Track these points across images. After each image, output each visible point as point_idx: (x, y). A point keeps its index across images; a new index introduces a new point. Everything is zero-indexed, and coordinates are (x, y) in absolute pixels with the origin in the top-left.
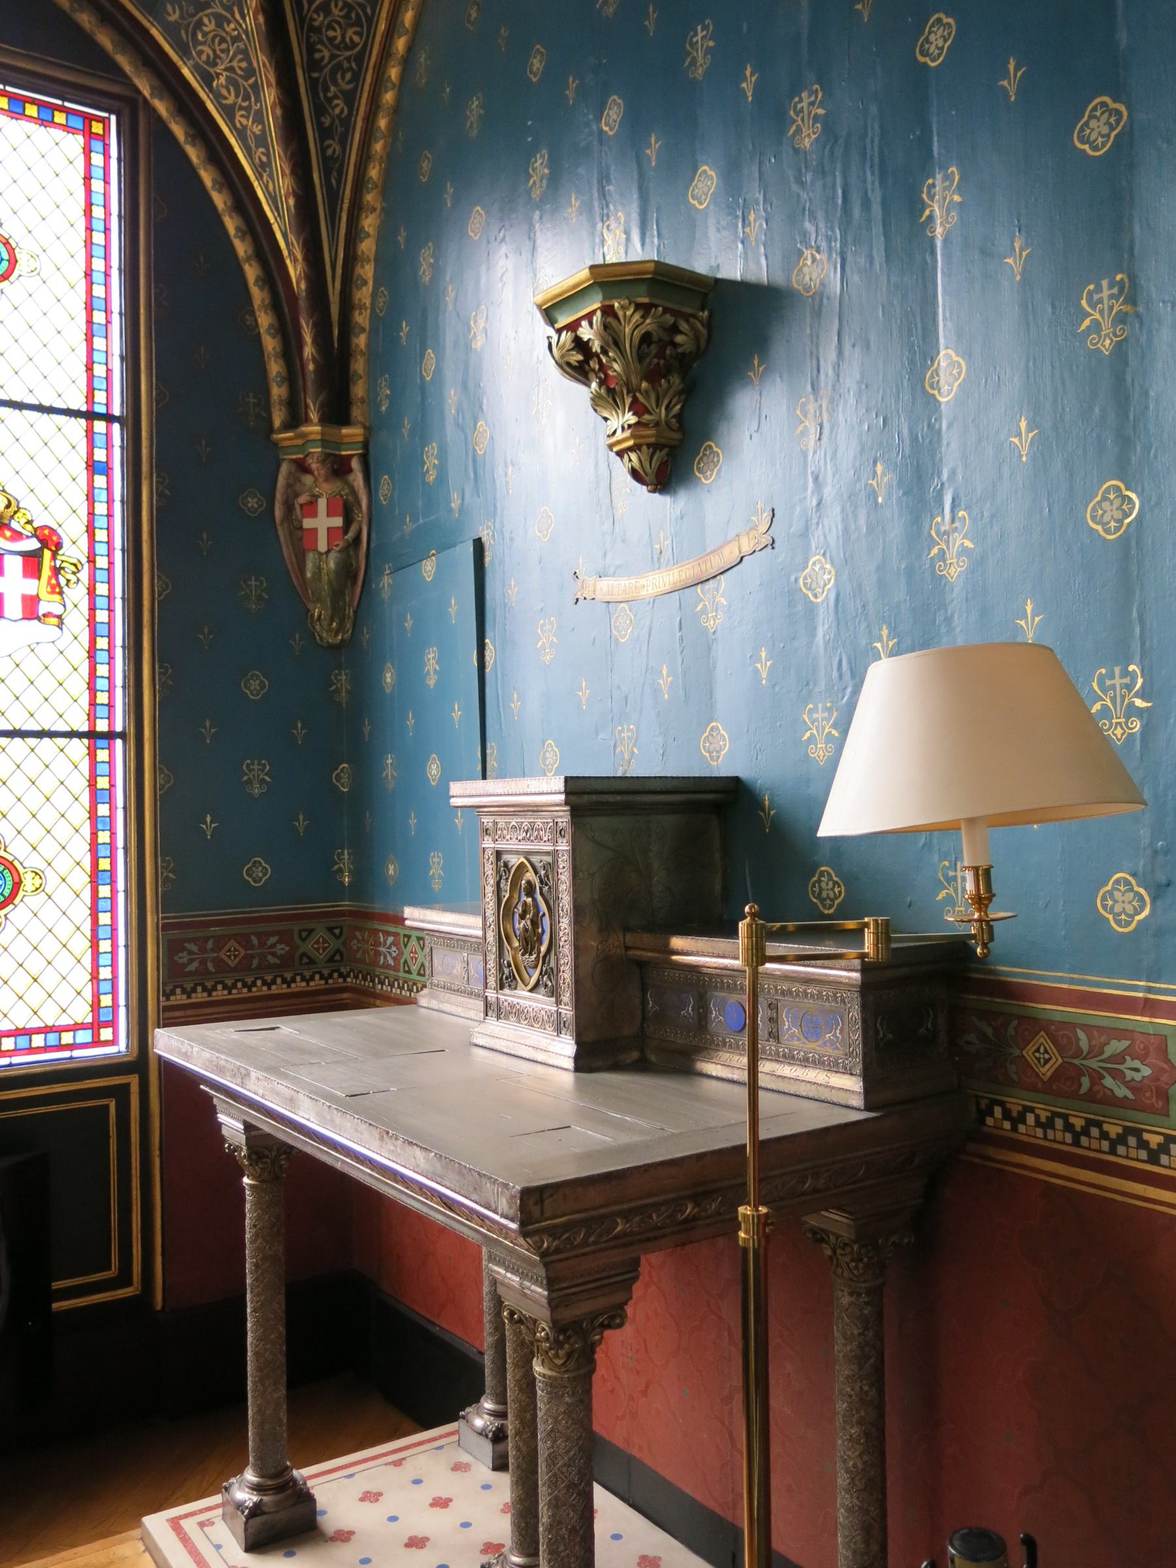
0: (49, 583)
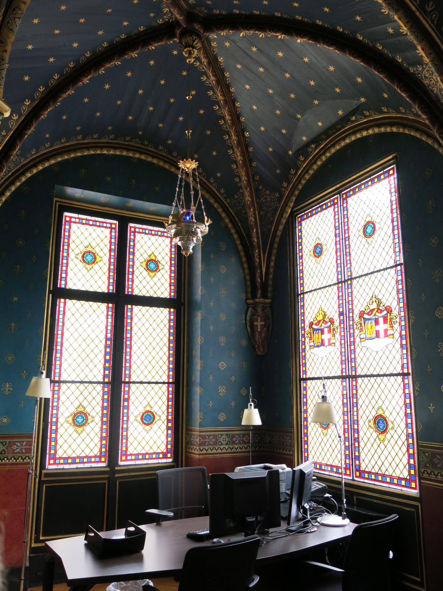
0: (389, 324)
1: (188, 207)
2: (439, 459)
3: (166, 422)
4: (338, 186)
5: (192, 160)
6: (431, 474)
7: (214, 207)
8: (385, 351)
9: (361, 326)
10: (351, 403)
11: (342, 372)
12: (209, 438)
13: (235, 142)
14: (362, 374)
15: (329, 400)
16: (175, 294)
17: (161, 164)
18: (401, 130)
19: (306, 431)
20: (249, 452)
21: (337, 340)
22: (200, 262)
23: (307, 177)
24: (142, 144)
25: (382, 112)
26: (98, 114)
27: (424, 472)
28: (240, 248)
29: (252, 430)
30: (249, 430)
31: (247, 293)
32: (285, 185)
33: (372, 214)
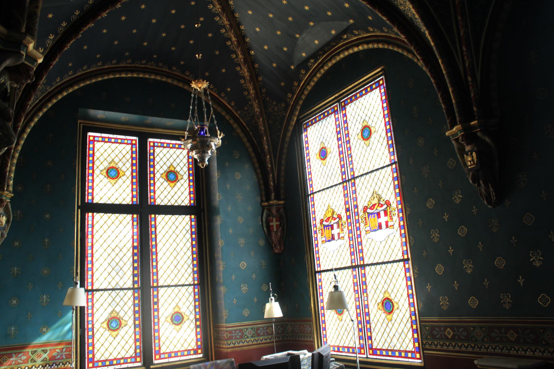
1: (201, 119)
2: (437, 331)
3: (194, 321)
4: (337, 95)
5: (203, 81)
6: (431, 344)
7: (226, 119)
8: (388, 241)
9: (366, 220)
10: (361, 288)
11: (352, 263)
12: (235, 333)
13: (242, 60)
14: (369, 263)
15: (341, 289)
16: (194, 202)
17: (175, 83)
18: (386, 47)
19: (323, 319)
20: (273, 342)
21: (345, 233)
22: (216, 171)
23: (309, 88)
24: (157, 66)
25: (368, 32)
26: (116, 43)
27: (426, 344)
28: (253, 154)
29: (275, 322)
30: (272, 323)
31: (261, 196)
32: (290, 95)
33: (367, 119)
